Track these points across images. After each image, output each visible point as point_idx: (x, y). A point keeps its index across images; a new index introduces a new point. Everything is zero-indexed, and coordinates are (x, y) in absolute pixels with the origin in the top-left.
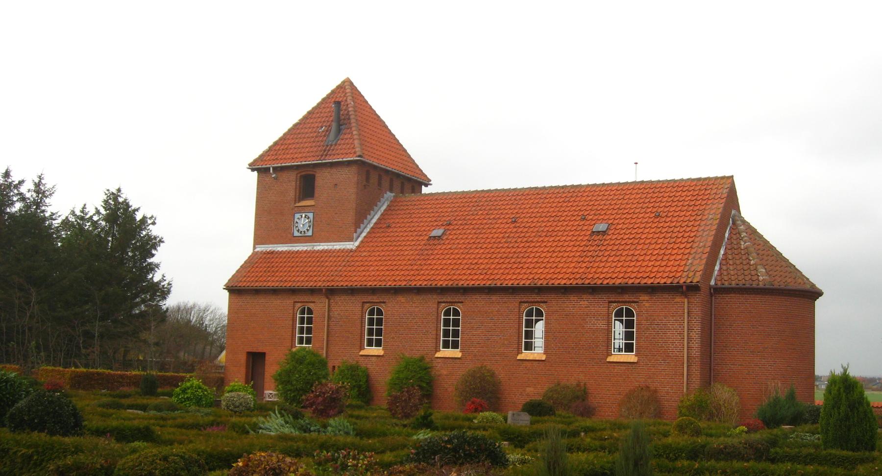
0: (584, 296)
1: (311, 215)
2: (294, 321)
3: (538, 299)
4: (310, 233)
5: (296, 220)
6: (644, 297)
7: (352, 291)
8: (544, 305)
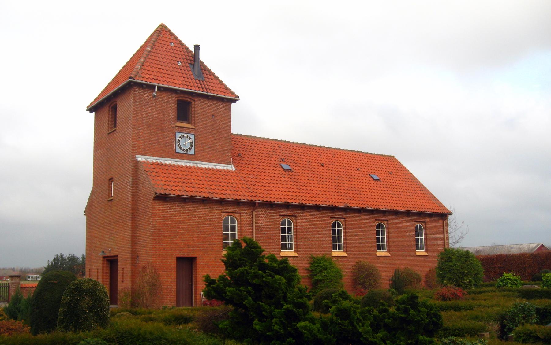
1: (192, 137)
2: (345, 239)
3: (384, 218)
4: (192, 152)
5: (178, 138)
7: (271, 206)
8: (237, 215)
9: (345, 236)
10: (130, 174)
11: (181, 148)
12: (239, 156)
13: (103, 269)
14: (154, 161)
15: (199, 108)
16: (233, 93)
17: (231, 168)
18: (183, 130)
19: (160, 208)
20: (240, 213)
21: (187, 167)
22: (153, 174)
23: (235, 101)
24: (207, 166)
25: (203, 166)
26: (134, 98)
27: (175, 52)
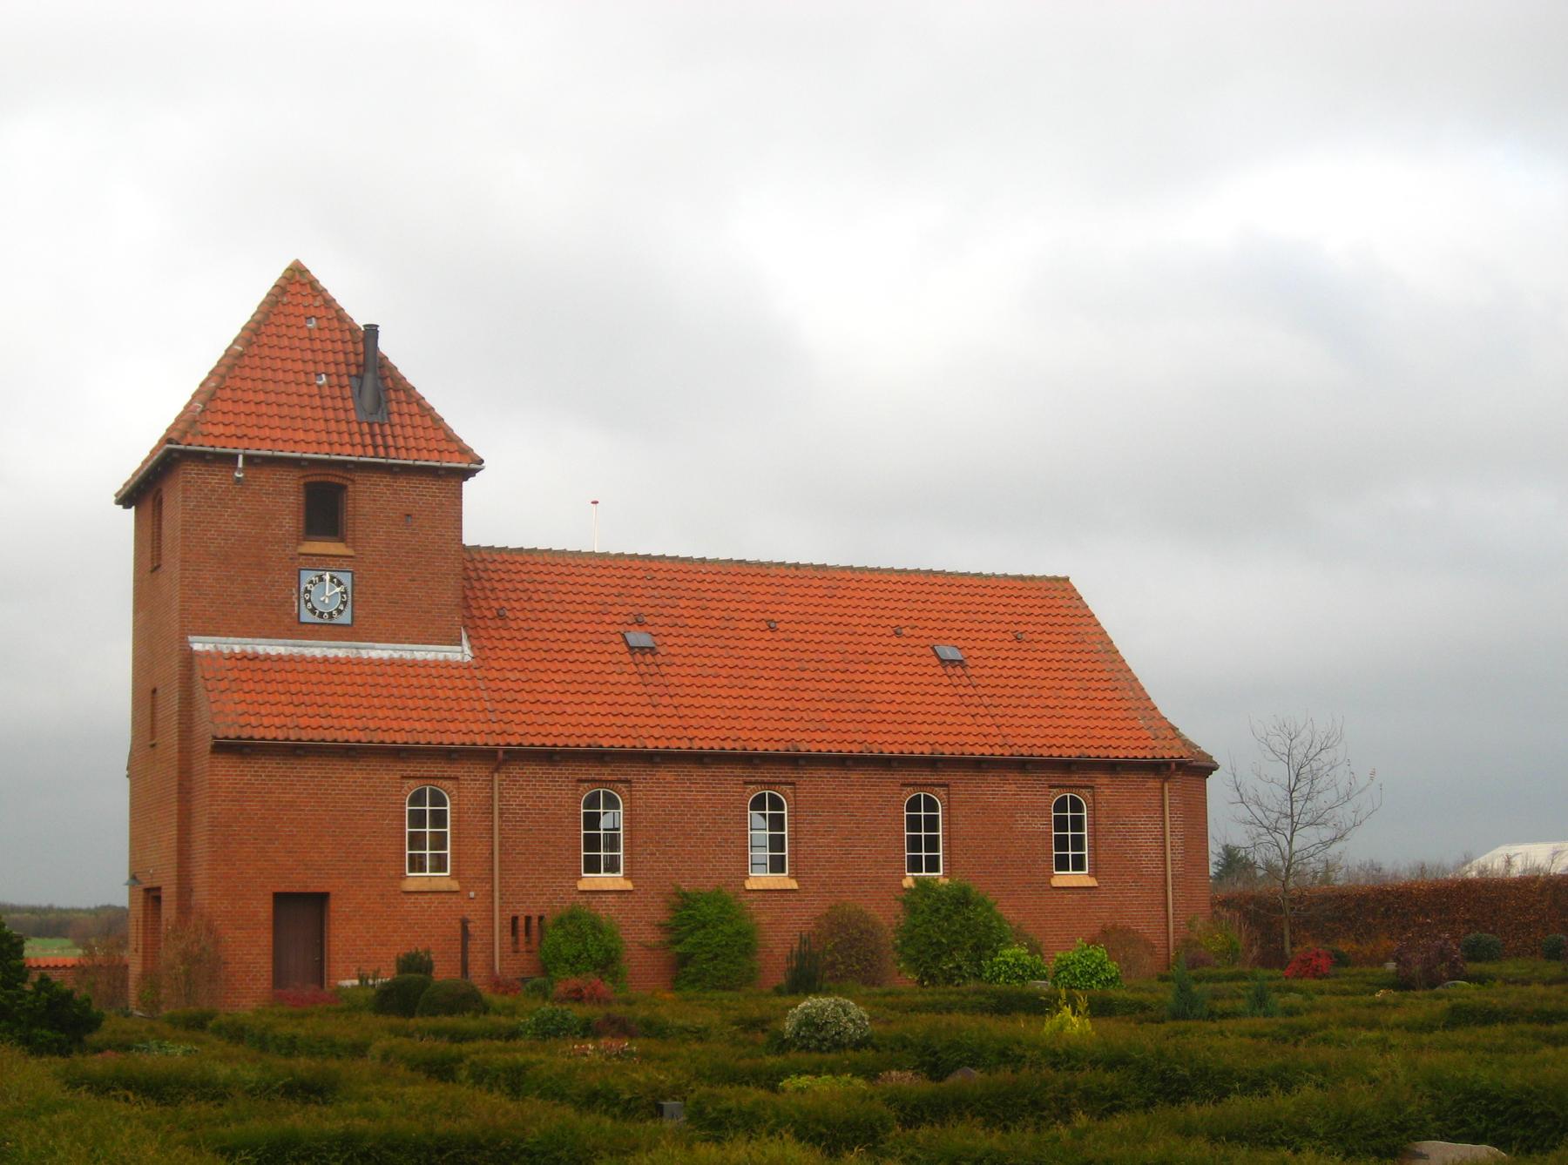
0: (1011, 776)
1: (346, 578)
3: (933, 779)
4: (346, 618)
6: (1102, 779)
8: (941, 791)
9: (795, 831)
10: (176, 684)
11: (313, 610)
12: (502, 617)
13: (145, 921)
14: (237, 649)
15: (368, 502)
16: (465, 451)
17: (462, 653)
18: (320, 562)
19: (228, 772)
20: (456, 778)
21: (326, 660)
22: (222, 686)
23: (468, 473)
24: (385, 655)
25: (375, 654)
26: (185, 490)
27: (317, 345)
